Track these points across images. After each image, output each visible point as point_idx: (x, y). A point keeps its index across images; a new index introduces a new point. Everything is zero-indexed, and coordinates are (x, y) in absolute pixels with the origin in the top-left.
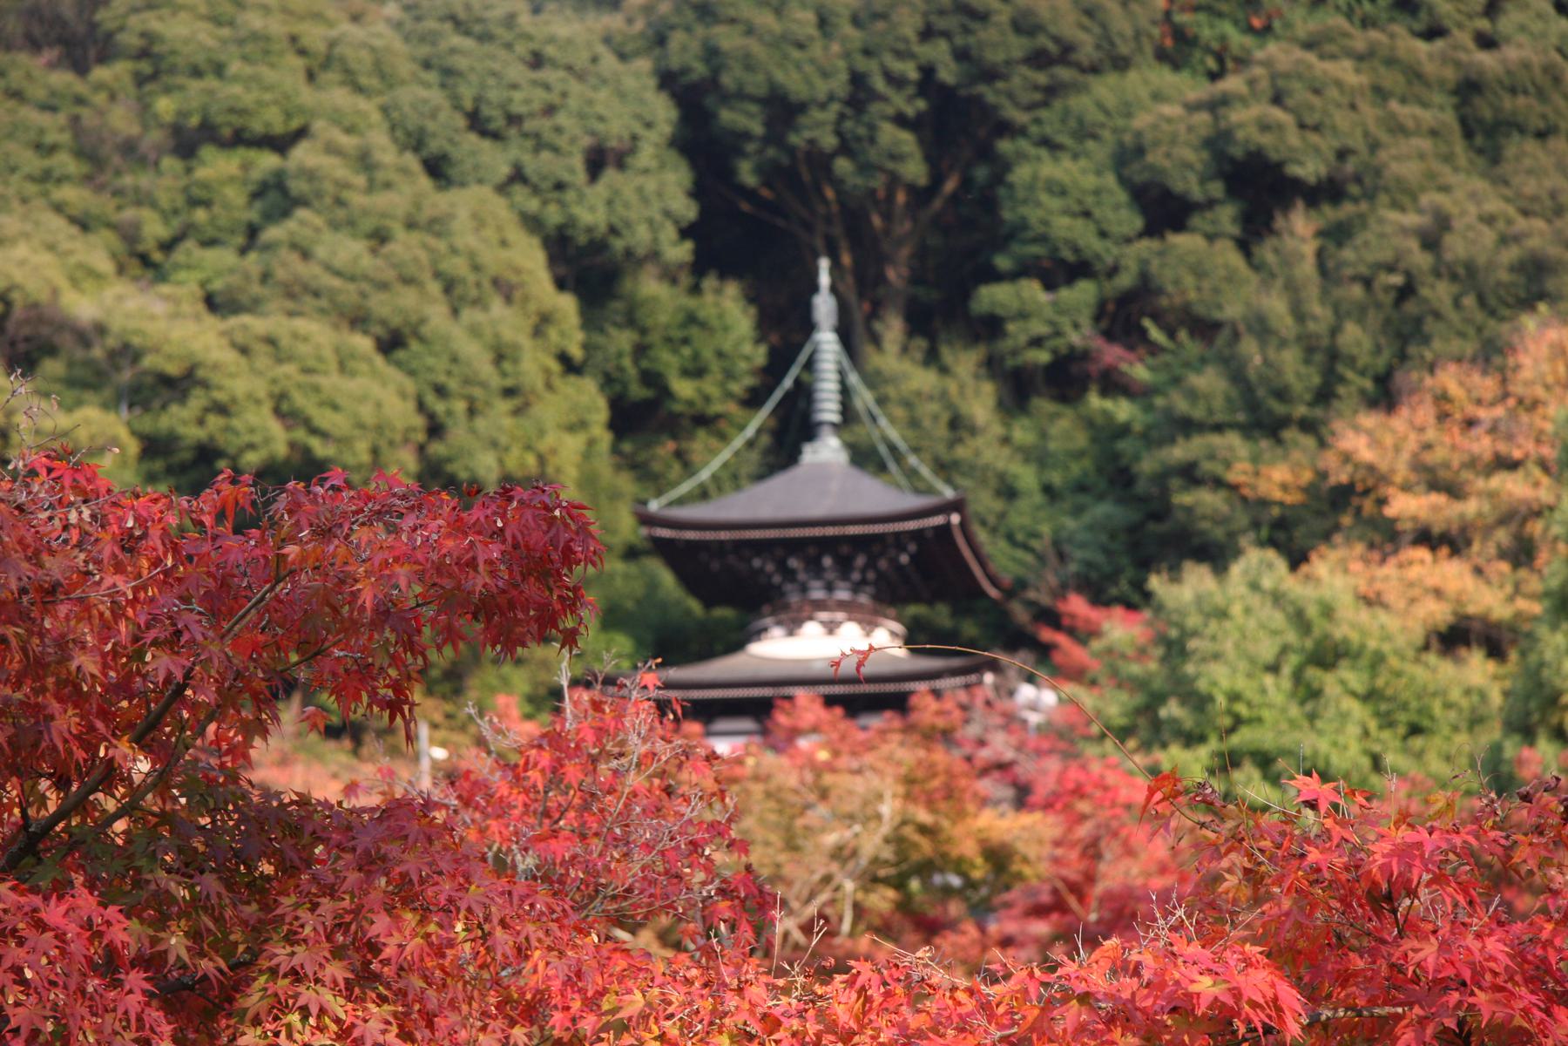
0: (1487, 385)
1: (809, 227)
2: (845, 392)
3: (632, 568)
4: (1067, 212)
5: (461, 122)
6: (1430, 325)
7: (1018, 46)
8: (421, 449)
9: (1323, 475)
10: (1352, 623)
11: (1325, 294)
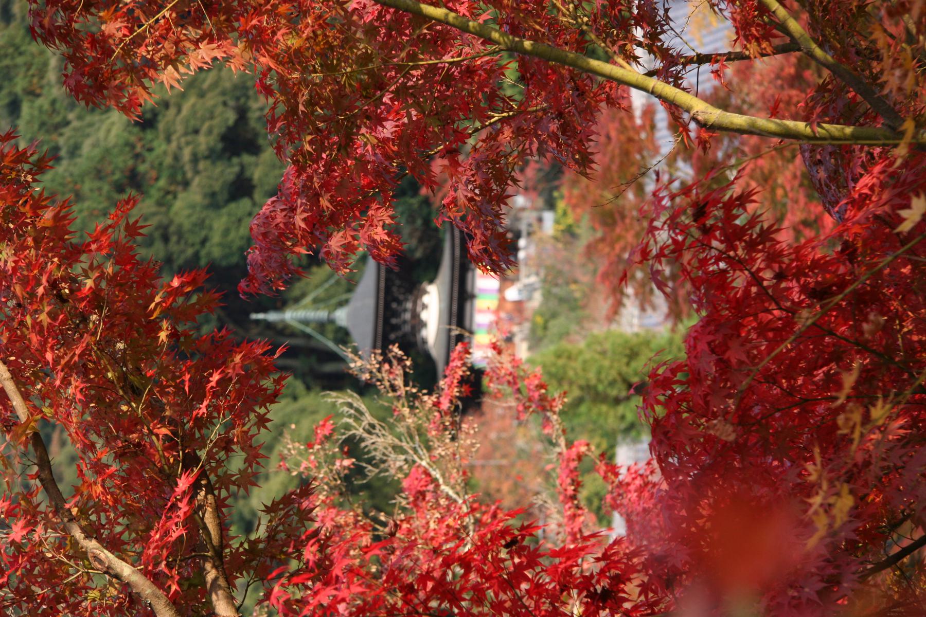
4: (238, 228)
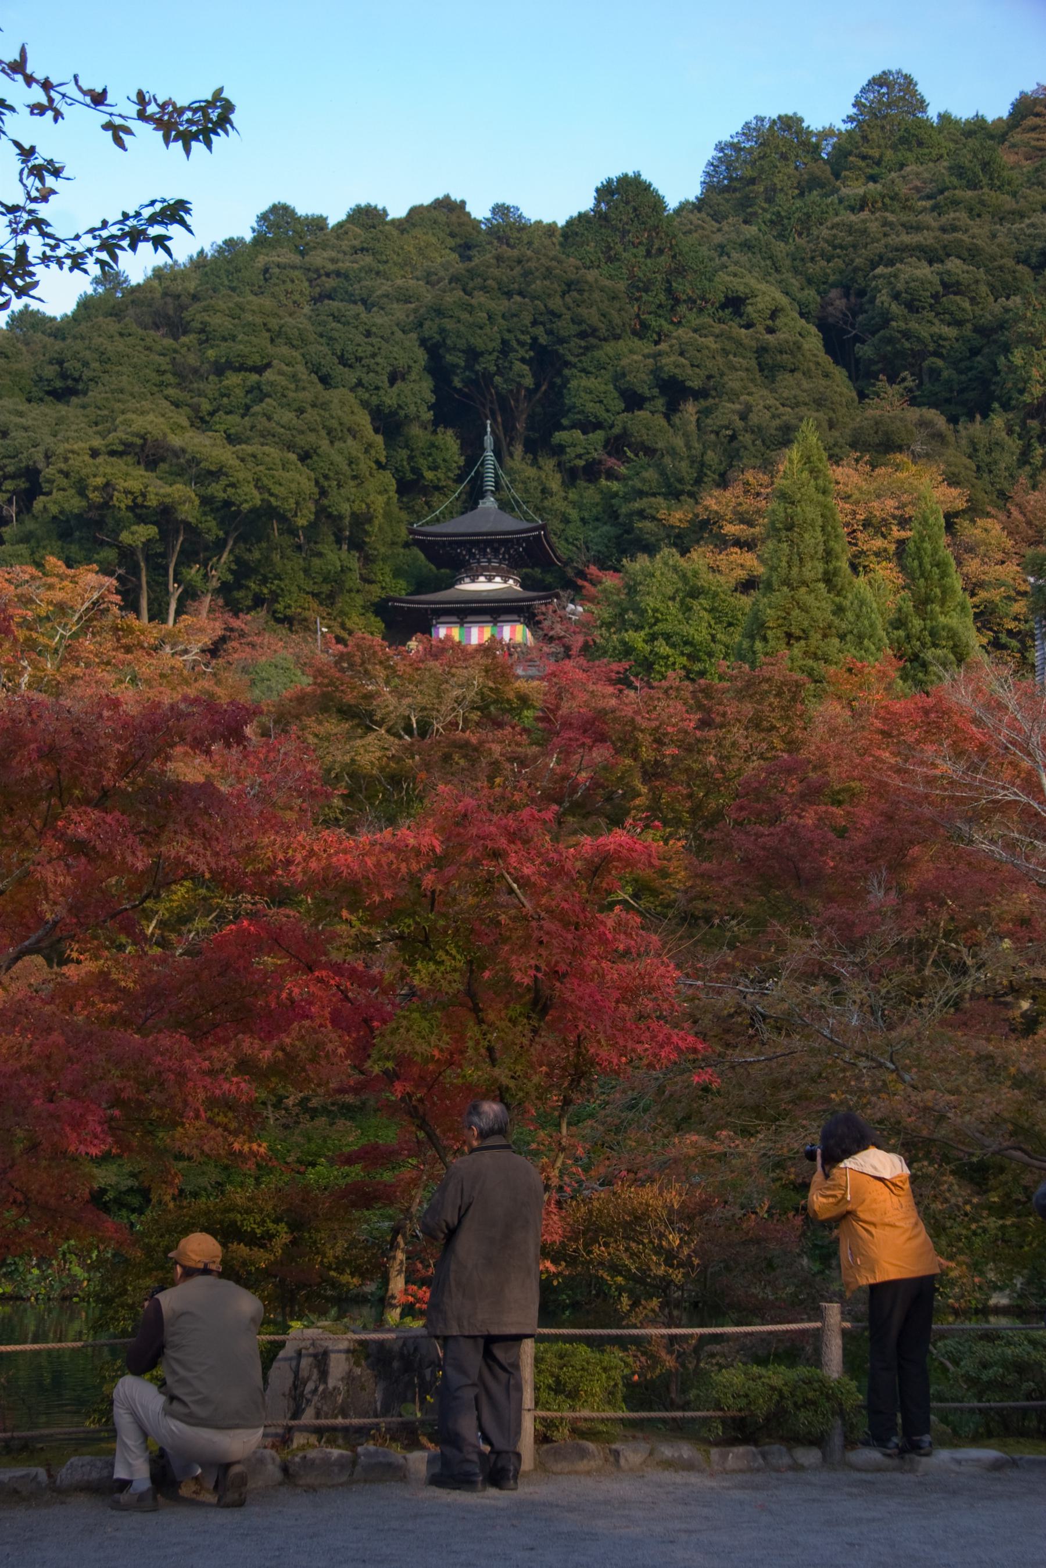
0: (765, 479)
1: (483, 405)
2: (497, 476)
3: (407, 551)
5: (336, 361)
6: (742, 452)
7: (574, 329)
8: (317, 502)
9: (697, 515)
10: (707, 579)
11: (699, 438)
